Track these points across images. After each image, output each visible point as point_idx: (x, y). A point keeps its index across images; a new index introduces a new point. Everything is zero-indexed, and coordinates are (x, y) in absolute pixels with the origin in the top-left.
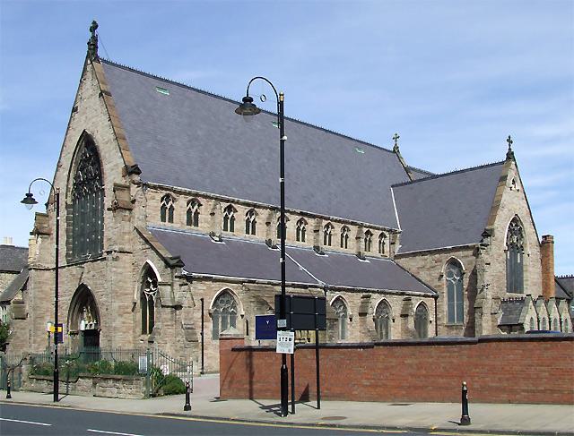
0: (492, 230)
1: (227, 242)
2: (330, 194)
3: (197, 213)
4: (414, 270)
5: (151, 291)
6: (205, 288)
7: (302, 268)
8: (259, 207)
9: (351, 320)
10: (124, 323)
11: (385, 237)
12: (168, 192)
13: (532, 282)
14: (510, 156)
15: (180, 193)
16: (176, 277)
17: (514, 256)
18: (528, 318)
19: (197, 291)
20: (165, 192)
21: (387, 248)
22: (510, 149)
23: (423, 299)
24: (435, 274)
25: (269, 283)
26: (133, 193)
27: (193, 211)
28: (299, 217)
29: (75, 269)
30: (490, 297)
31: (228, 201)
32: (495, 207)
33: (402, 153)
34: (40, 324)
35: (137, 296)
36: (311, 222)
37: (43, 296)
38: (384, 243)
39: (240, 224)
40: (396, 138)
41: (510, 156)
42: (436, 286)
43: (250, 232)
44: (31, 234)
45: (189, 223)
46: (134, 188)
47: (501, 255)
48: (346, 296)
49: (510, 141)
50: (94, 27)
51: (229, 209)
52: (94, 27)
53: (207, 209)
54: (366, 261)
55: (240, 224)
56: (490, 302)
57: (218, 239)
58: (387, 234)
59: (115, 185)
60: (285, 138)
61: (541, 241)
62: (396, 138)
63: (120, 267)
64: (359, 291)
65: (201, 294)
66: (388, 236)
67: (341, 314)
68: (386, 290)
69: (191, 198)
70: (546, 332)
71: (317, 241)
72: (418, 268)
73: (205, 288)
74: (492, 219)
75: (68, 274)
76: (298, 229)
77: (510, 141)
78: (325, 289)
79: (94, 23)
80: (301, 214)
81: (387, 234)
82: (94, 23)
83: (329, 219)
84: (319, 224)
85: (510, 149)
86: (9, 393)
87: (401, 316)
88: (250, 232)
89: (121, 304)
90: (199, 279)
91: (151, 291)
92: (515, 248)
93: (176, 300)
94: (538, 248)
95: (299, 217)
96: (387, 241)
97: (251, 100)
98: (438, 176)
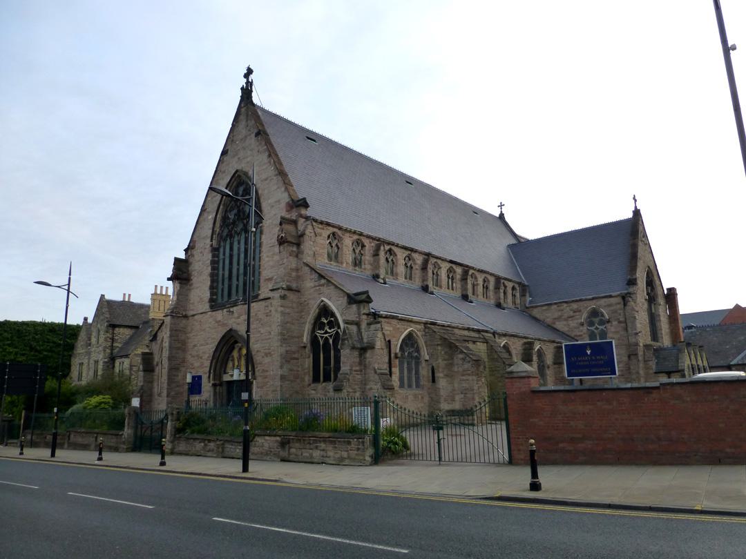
0: (636, 279)
4: (549, 321)
5: (326, 332)
10: (291, 370)
16: (364, 314)
20: (331, 230)
21: (518, 301)
22: (636, 207)
26: (301, 227)
30: (641, 345)
33: (507, 219)
34: (174, 375)
35: (306, 338)
37: (179, 345)
40: (501, 206)
44: (169, 279)
46: (302, 221)
52: (250, 71)
57: (382, 282)
59: (282, 218)
61: (666, 292)
62: (501, 206)
71: (466, 289)
75: (210, 320)
85: (636, 207)
86: (100, 454)
87: (555, 364)
89: (288, 348)
91: (326, 332)
92: (652, 299)
93: (365, 340)
96: (518, 295)
97: (304, 204)
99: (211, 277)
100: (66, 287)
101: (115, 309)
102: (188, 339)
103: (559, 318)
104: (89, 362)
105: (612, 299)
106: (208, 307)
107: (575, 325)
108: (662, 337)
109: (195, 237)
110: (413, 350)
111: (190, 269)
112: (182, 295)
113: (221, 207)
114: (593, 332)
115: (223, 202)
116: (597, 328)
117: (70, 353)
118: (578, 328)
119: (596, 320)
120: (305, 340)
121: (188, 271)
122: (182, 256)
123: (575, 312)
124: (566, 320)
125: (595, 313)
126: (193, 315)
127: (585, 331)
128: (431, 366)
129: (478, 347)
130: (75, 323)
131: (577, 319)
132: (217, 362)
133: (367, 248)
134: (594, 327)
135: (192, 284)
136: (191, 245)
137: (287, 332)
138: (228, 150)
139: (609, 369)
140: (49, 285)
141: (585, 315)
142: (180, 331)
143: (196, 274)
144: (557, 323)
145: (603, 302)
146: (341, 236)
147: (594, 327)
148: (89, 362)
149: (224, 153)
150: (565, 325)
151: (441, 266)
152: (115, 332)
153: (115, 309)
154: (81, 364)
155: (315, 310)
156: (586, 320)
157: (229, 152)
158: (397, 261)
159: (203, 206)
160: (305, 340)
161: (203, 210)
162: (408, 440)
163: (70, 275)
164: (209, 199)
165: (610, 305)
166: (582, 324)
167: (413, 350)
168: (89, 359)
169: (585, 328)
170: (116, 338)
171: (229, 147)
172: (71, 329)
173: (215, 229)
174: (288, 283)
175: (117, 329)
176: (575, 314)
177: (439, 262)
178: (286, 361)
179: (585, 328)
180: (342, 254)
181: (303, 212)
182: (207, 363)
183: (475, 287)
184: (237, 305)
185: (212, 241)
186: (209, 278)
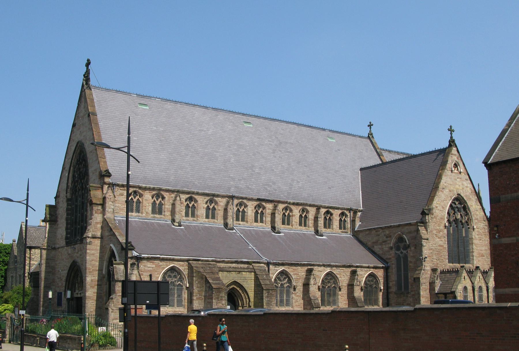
1: (187, 227)
2: (293, 180)
3: (161, 204)
6: (154, 266)
7: (251, 246)
8: (218, 196)
9: (464, 278)
11: (346, 216)
12: (135, 189)
13: (479, 254)
14: (452, 143)
15: (145, 189)
17: (457, 231)
18: (460, 287)
19: (146, 269)
22: (451, 137)
23: (372, 271)
24: (386, 248)
25: (213, 261)
27: (158, 202)
28: (256, 203)
29: (69, 250)
31: (188, 193)
32: (435, 188)
36: (269, 207)
38: (345, 221)
39: (201, 211)
41: (452, 143)
42: (387, 258)
43: (210, 216)
44: (43, 221)
45: (154, 212)
47: (440, 231)
48: (289, 270)
49: (451, 130)
50: (88, 64)
51: (191, 199)
52: (88, 64)
53: (169, 200)
54: (324, 237)
55: (201, 211)
56: (429, 273)
58: (347, 213)
60: (130, 173)
62: (370, 126)
63: (92, 250)
64: (304, 265)
65: (150, 271)
66: (349, 214)
67: (285, 286)
68: (332, 264)
69: (154, 192)
70: (469, 302)
72: (373, 243)
73: (154, 266)
74: (431, 198)
76: (257, 213)
77: (451, 130)
78: (268, 264)
79: (88, 60)
80: (259, 200)
81: (347, 213)
82: (88, 60)
83: (286, 203)
84: (275, 207)
85: (451, 137)
88: (210, 216)
90: (148, 259)
94: (486, 223)
95: (256, 203)
98: (415, 156)
99: (66, 221)
100: (25, 202)
101: (33, 233)
102: (56, 265)
103: (376, 243)
104: (16, 275)
105: (411, 227)
106: (65, 243)
107: (387, 249)
108: (473, 259)
109: (60, 188)
110: (176, 279)
111: (57, 212)
112: (52, 233)
113: (72, 168)
114: (399, 256)
115: (72, 165)
116: (402, 253)
117: (150, 224)
118: (389, 251)
119: (402, 245)
120: (104, 272)
121: (56, 214)
122: (53, 203)
123: (387, 237)
124: (381, 244)
125: (401, 239)
126: (59, 248)
127: (393, 255)
128: (190, 292)
129: (243, 276)
130: (9, 243)
131: (389, 244)
132: (69, 284)
133: (167, 199)
134: (400, 252)
135: (58, 225)
136: (58, 194)
137: (92, 267)
138: (76, 123)
139: (133, 306)
140: (162, 99)
141: (393, 240)
142: (51, 259)
143: (60, 217)
144: (375, 247)
145: (406, 229)
146: (142, 193)
147: (400, 252)
148: (16, 275)
149: (74, 125)
150: (380, 249)
151: (248, 204)
152: (32, 252)
153: (33, 233)
154: (12, 277)
155: (108, 252)
156: (394, 244)
157: (76, 125)
158: (197, 206)
159: (64, 165)
160: (104, 272)
161: (63, 168)
162: (117, 340)
163: (28, 190)
164: (67, 160)
165: (410, 232)
166: (391, 248)
167: (176, 279)
168: (16, 273)
169: (393, 252)
170: (33, 257)
171: (76, 122)
172: (82, 215)
173: (69, 185)
174: (93, 233)
175: (33, 250)
176: (387, 239)
177: (245, 201)
178: (91, 287)
179: (393, 252)
180: (142, 207)
181: (107, 180)
182: (64, 283)
183: (291, 218)
184: (77, 244)
185: (66, 193)
186: (65, 222)
